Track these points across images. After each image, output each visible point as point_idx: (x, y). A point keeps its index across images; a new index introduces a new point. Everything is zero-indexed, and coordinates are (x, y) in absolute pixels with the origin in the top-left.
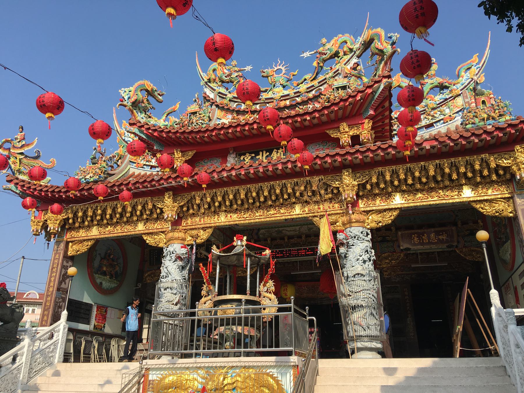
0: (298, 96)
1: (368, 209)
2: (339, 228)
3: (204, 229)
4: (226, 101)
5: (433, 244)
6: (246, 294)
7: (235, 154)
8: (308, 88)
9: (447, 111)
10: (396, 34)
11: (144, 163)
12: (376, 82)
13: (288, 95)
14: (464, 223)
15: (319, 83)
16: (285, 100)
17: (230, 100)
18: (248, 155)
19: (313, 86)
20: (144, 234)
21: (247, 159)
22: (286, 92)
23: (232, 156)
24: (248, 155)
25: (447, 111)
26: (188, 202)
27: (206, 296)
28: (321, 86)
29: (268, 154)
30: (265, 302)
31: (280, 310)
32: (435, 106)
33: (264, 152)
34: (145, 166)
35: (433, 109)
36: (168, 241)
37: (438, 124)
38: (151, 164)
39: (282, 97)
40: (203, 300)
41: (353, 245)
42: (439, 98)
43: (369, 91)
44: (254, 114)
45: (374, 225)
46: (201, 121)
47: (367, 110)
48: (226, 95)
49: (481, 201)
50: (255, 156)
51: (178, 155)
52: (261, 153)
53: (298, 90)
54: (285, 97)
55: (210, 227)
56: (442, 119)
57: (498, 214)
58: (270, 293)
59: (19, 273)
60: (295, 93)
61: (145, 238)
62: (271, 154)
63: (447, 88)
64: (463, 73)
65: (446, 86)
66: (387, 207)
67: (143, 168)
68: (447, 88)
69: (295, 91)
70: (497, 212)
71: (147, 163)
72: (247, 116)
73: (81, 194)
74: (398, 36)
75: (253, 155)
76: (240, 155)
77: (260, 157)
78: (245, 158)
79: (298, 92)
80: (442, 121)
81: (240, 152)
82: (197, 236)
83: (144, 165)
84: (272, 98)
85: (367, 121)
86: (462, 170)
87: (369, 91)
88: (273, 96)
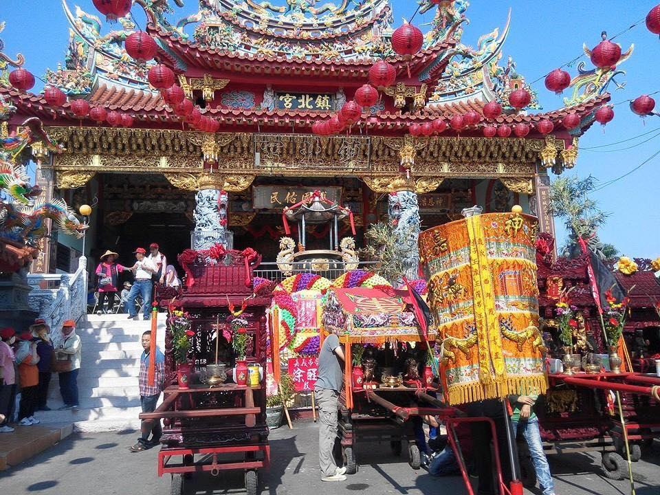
0: (323, 30)
1: (419, 175)
2: (390, 191)
3: (245, 176)
4: (231, 13)
5: (431, 207)
6: (329, 249)
7: (273, 92)
8: (334, 22)
9: (469, 82)
10: (466, 2)
11: (120, 74)
12: (442, 48)
13: (311, 25)
14: (456, 191)
15: (347, 19)
16: (307, 30)
17: (238, 14)
18: (288, 96)
19: (340, 21)
20: (167, 173)
21: (288, 101)
22: (309, 21)
23: (270, 94)
24: (288, 96)
25: (469, 82)
26: (230, 144)
27: (284, 249)
28: (349, 23)
29: (312, 99)
30: (347, 257)
31: (360, 266)
32: (459, 74)
33: (308, 96)
34: (120, 79)
35: (458, 77)
36: (202, 185)
37: (460, 94)
38: (130, 77)
39: (304, 25)
40: (282, 253)
41: (405, 208)
42: (464, 67)
43: (435, 56)
44: (270, 40)
45: (421, 191)
46: (227, 41)
47: (423, 73)
48: (232, 6)
49: (508, 178)
50: (297, 99)
51: (207, 79)
52: (303, 97)
53: (322, 22)
54: (307, 27)
55: (252, 174)
56: (464, 90)
57: (520, 191)
58: (351, 249)
59: (331, 236)
60: (319, 25)
61: (169, 178)
62: (315, 99)
63: (471, 57)
64: (484, 46)
65: (470, 56)
66: (435, 175)
67: (118, 80)
68: (471, 57)
69: (319, 22)
70: (519, 189)
71: (124, 75)
72: (260, 39)
73: (66, 113)
74: (468, 5)
75: (295, 97)
76: (280, 95)
77: (303, 101)
78: (285, 99)
79: (323, 24)
80: (464, 92)
81: (279, 91)
82: (236, 184)
83: (120, 77)
84: (292, 25)
85: (423, 85)
86: (504, 150)
87: (435, 56)
88: (292, 22)
